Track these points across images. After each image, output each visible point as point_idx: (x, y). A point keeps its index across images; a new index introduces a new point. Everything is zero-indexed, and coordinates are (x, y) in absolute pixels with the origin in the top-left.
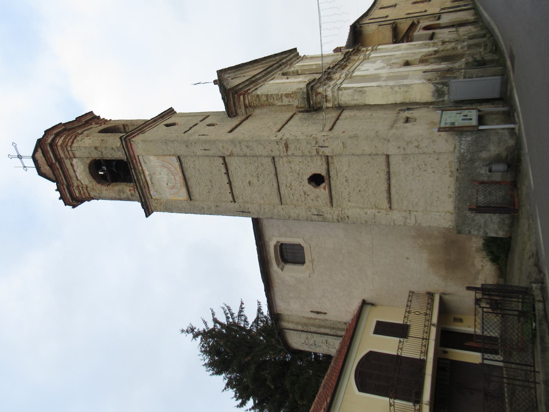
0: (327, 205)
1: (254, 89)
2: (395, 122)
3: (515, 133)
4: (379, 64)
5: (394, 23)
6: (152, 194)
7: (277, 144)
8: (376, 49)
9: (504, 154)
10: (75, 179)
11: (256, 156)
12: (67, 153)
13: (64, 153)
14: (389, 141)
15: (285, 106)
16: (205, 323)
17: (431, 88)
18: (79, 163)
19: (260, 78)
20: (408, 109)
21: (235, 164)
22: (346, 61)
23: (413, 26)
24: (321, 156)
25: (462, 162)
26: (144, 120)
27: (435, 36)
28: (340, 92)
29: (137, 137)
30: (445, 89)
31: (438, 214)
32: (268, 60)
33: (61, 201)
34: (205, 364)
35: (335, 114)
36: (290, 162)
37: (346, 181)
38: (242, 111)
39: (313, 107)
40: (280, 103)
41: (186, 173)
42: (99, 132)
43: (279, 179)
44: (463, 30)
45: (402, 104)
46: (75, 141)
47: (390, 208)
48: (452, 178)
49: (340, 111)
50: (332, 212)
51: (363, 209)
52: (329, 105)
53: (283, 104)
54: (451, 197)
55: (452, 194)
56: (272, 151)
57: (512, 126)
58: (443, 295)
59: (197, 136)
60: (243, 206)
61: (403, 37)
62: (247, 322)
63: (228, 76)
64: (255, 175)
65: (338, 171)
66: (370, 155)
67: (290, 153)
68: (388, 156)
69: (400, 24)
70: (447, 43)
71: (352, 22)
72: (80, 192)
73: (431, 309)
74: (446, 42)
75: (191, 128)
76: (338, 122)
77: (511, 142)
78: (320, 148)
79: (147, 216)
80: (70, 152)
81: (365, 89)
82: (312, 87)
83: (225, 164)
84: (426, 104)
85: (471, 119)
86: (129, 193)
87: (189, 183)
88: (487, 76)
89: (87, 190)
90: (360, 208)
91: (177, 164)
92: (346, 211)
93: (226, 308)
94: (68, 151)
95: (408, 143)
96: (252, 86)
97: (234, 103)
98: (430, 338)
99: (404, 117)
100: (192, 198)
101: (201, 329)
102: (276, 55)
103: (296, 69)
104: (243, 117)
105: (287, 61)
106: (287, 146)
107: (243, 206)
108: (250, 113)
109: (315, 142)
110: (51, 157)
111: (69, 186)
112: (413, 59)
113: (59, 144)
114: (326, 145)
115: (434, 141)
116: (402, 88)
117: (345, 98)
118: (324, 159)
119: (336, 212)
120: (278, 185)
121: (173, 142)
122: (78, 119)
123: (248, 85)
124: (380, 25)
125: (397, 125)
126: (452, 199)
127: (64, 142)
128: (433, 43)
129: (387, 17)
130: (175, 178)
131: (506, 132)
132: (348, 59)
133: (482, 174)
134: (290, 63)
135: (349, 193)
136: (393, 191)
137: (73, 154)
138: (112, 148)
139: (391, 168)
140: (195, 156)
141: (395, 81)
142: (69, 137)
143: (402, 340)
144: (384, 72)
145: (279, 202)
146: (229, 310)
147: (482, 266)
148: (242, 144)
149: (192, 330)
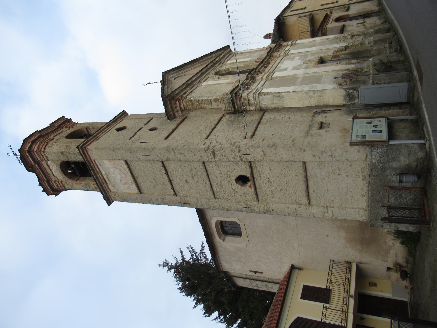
0: (254, 200)
1: (189, 92)
2: (310, 127)
3: (425, 148)
4: (297, 62)
5: (311, 14)
6: (110, 188)
7: (205, 152)
8: (295, 44)
9: (414, 164)
10: (52, 175)
11: (189, 161)
12: (42, 157)
13: (40, 158)
14: (304, 150)
15: (215, 109)
16: (176, 259)
17: (343, 92)
18: (53, 164)
19: (196, 80)
20: (323, 112)
21: (172, 167)
22: (269, 58)
23: (327, 17)
24: (245, 161)
25: (373, 170)
26: (102, 123)
27: (345, 29)
28: (261, 98)
29: (92, 145)
30: (356, 93)
31: (353, 210)
32: (205, 59)
33: (44, 193)
34: (180, 288)
35: (257, 117)
36: (218, 166)
37: (269, 181)
38: (179, 114)
39: (238, 111)
40: (210, 107)
41: (134, 173)
42: (68, 137)
43: (211, 179)
44: (369, 21)
45: (317, 107)
46: (47, 147)
47: (309, 203)
48: (365, 182)
49: (262, 113)
50: (259, 205)
51: (285, 204)
52: (252, 108)
53: (213, 107)
54: (364, 196)
55: (365, 194)
56: (201, 157)
57: (422, 141)
58: (359, 264)
59: (139, 143)
60: (183, 199)
61: (318, 30)
62: (207, 259)
63: (172, 76)
64: (190, 175)
65: (261, 174)
66: (288, 161)
67: (217, 159)
68: (304, 163)
69: (316, 15)
70: (356, 37)
71: (276, 16)
72: (57, 186)
73: (349, 279)
74: (355, 35)
75: (136, 133)
76: (259, 126)
77: (421, 155)
78: (243, 155)
79: (109, 205)
80: (44, 156)
81: (283, 94)
82: (236, 94)
83: (164, 166)
84: (339, 107)
85: (381, 131)
86: (94, 187)
87: (138, 181)
88: (394, 82)
89: (62, 184)
90: (283, 203)
91: (125, 166)
92: (271, 205)
93: (190, 248)
94: (42, 156)
95: (322, 152)
96: (188, 89)
97: (172, 107)
98: (349, 311)
99: (319, 121)
100: (142, 191)
101: (174, 264)
102: (212, 53)
103: (227, 67)
104: (181, 119)
105: (220, 59)
106: (214, 154)
107: (183, 199)
108: (186, 115)
109: (238, 151)
110: (30, 161)
111: (49, 181)
112: (326, 55)
113: (35, 150)
114: (248, 152)
115: (346, 151)
116: (316, 93)
117: (265, 102)
118: (247, 164)
119: (262, 206)
120: (211, 184)
121: (119, 149)
122: (52, 125)
123: (185, 88)
124: (299, 17)
125: (312, 132)
126: (365, 198)
127: (38, 148)
128: (344, 37)
129: (305, 8)
130: (126, 177)
131: (415, 145)
132: (270, 56)
133: (393, 180)
134: (222, 61)
135: (272, 191)
136: (311, 191)
137: (47, 158)
138: (74, 153)
139: (308, 172)
140: (139, 160)
141: (309, 85)
142: (43, 144)
143: (326, 305)
144: (300, 72)
145: (213, 197)
146: (193, 249)
147: (393, 244)
148: (175, 152)
149: (167, 264)
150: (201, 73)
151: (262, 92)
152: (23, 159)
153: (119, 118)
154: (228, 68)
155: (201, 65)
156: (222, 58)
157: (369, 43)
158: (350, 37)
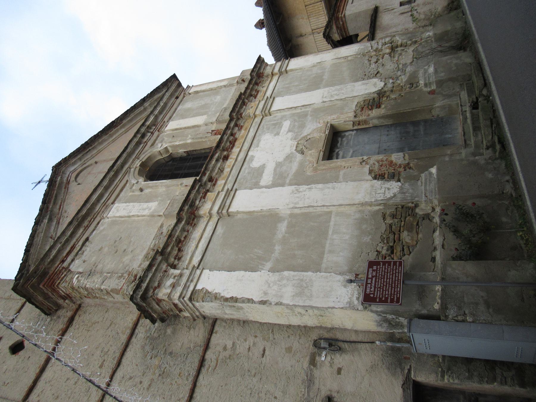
8: (286, 72)
32: (132, 115)
74: (397, 47)
76: (201, 377)
96: (81, 230)
102: (144, 100)
150: (112, 173)
151: (197, 288)
154: (166, 148)
155: (126, 132)
156: (160, 113)
157: (426, 85)
158: (388, 51)
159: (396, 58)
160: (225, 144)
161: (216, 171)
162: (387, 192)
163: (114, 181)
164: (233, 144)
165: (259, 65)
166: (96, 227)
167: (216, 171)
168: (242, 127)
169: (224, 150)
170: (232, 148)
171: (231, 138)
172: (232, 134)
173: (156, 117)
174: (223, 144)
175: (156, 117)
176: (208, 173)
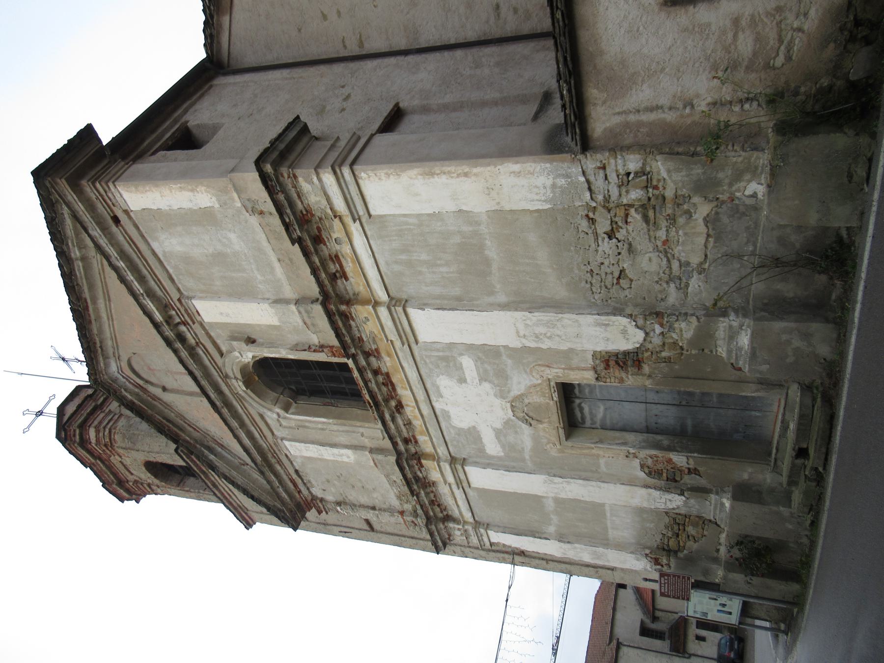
85: (730, 613)
150: (225, 411)
152: (64, 434)
153: (231, 504)
159: (662, 234)
160: (382, 394)
161: (404, 430)
162: (668, 503)
163: (236, 412)
164: (388, 382)
165: (281, 197)
166: (289, 460)
167: (404, 430)
168: (377, 350)
169: (387, 401)
170: (394, 389)
171: (380, 379)
172: (376, 372)
173: (150, 294)
174: (379, 396)
175: (150, 294)
176: (399, 440)
